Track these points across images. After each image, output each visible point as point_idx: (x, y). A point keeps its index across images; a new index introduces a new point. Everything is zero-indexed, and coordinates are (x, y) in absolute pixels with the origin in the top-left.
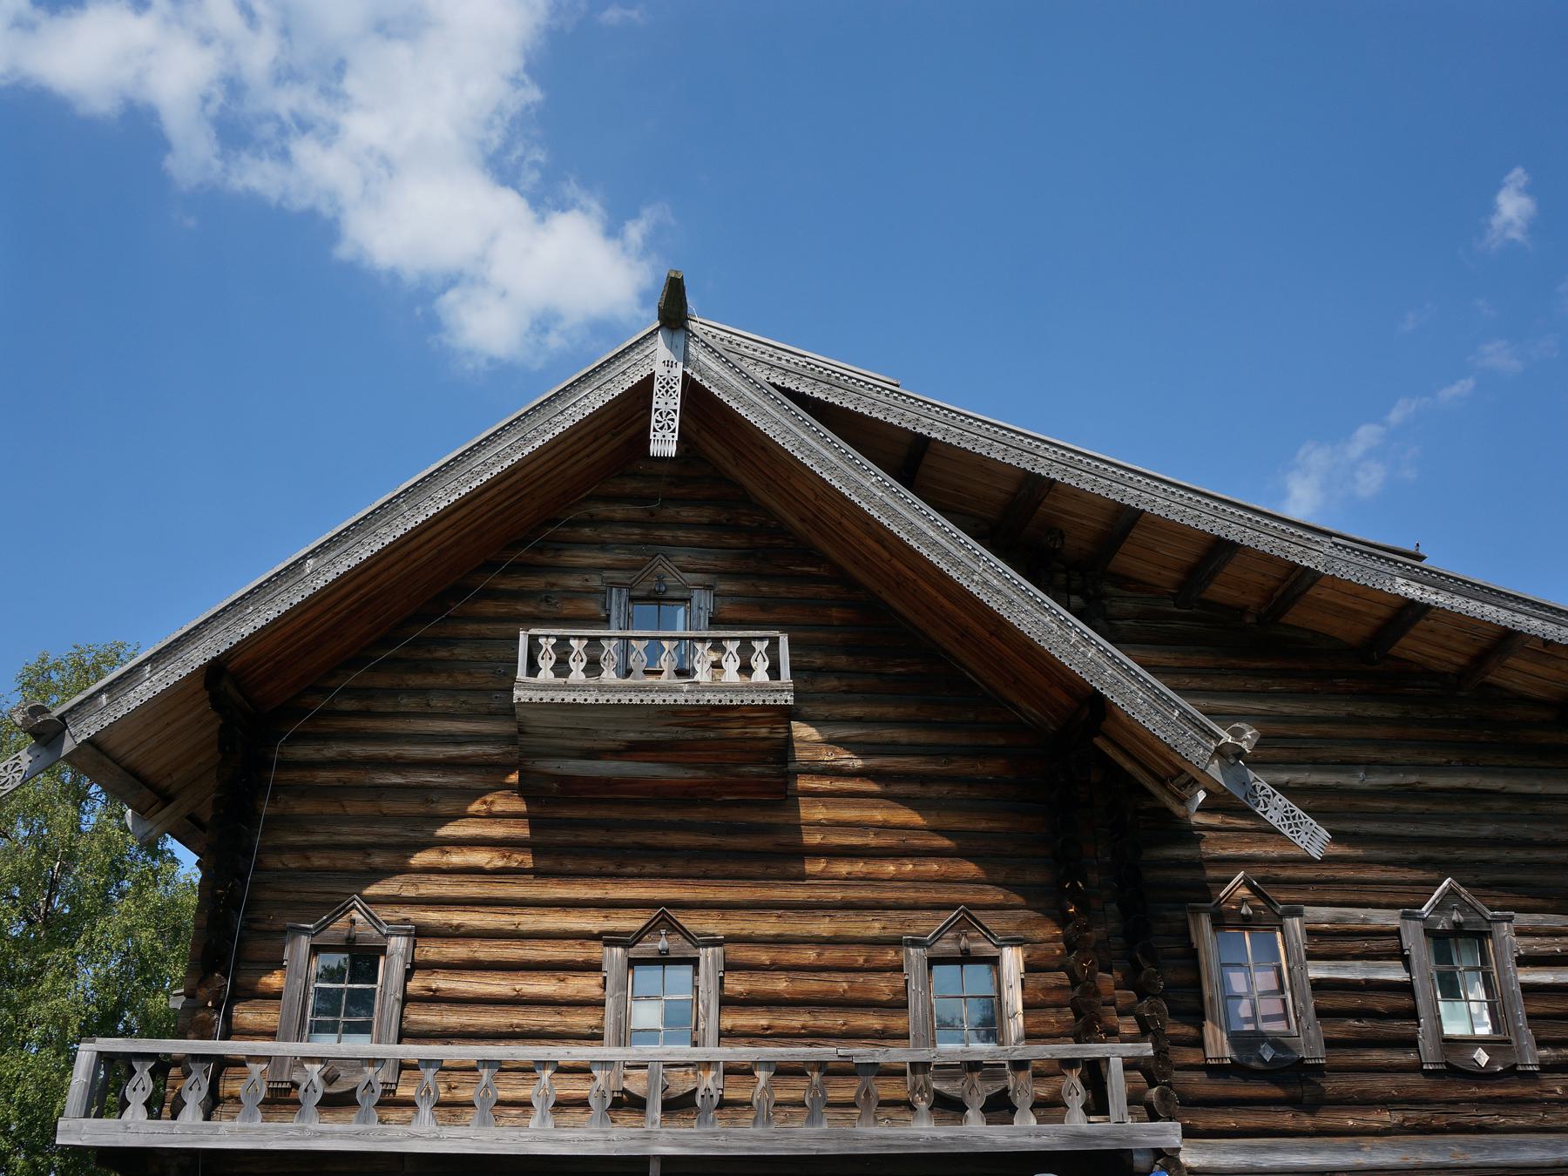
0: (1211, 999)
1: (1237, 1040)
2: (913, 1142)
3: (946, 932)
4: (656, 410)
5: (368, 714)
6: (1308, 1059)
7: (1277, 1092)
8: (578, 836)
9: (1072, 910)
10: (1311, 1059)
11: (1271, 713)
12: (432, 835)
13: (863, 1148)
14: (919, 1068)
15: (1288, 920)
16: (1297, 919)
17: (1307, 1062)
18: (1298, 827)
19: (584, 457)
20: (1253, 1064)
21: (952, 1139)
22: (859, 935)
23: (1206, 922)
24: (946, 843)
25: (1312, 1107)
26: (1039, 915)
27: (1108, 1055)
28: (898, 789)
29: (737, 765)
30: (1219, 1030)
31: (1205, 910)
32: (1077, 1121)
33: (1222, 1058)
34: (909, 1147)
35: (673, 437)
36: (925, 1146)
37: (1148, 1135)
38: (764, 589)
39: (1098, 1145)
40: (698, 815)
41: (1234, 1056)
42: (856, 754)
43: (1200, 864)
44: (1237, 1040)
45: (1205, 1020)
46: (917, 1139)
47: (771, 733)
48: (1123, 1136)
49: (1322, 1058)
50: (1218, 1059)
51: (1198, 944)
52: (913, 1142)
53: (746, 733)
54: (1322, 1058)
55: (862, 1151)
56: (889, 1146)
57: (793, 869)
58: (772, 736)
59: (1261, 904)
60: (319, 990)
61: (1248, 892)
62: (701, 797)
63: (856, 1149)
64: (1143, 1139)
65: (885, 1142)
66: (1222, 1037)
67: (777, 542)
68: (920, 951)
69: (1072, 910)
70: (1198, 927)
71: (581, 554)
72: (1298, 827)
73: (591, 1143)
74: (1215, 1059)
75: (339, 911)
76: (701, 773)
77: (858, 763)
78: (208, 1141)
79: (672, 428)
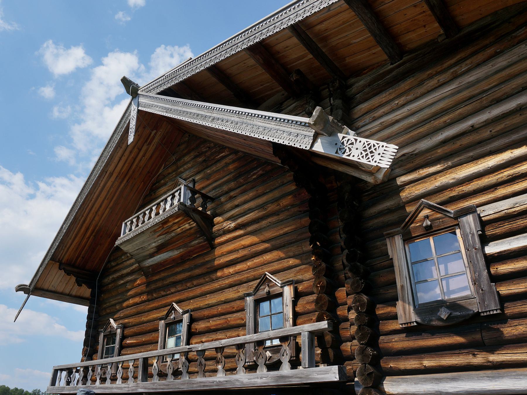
0: (402, 287)
1: (420, 309)
2: (212, 384)
3: (260, 287)
4: (356, 140)
5: (118, 265)
6: (483, 312)
7: (459, 339)
8: (156, 285)
9: (314, 258)
10: (486, 312)
11: (461, 88)
12: (126, 296)
13: (195, 387)
14: (219, 350)
15: (464, 219)
16: (471, 216)
17: (482, 314)
18: (371, 146)
19: (142, 158)
20: (434, 323)
21: (226, 381)
22: (233, 297)
23: (398, 240)
24: (267, 245)
25: (492, 349)
26: (307, 266)
27: (301, 332)
28: (250, 229)
29: (190, 242)
30: (407, 305)
31: (397, 233)
32: (286, 370)
33: (410, 323)
34: (210, 386)
35: (383, 146)
36: (216, 385)
37: (318, 374)
38: (208, 172)
39: (290, 381)
40: (186, 266)
41: (419, 320)
42: (232, 221)
43: (401, 207)
44: (420, 309)
45: (398, 300)
46: (213, 382)
47: (190, 225)
48: (303, 376)
49: (496, 310)
50: (407, 323)
51: (393, 255)
52: (212, 384)
53: (183, 229)
54: (496, 310)
55: (195, 388)
56: (204, 386)
57: (214, 276)
58: (191, 226)
59: (439, 215)
60: (106, 348)
61: (430, 211)
62: (186, 259)
63: (193, 387)
64: (314, 376)
65: (202, 384)
66: (409, 309)
67: (213, 151)
68: (251, 298)
69: (314, 258)
70: (393, 244)
71: (161, 190)
72: (371, 146)
73: (125, 388)
74: (405, 324)
75: (107, 324)
76: (181, 250)
77: (233, 225)
78: (63, 391)
79: (354, 141)
